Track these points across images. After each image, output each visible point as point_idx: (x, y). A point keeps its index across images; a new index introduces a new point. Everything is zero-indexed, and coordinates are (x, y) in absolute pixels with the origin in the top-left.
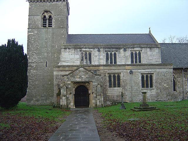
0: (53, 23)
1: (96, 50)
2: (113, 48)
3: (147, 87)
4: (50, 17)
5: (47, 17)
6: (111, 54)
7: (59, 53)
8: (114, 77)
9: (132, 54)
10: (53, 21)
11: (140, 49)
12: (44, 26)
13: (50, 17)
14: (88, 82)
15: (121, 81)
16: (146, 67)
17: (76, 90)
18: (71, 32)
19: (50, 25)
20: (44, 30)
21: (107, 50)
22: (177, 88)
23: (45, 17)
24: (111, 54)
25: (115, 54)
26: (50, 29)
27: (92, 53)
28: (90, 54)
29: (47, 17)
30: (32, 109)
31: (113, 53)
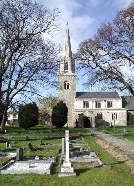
0: (69, 87)
1: (91, 101)
2: (99, 100)
3: (98, 107)
4: (68, 84)
5: (67, 84)
6: (98, 103)
7: (73, 102)
8: (100, 114)
9: (108, 103)
10: (70, 86)
11: (112, 101)
12: (65, 88)
13: (68, 84)
14: (90, 117)
15: (103, 116)
16: (114, 110)
17: (84, 121)
18: (126, 125)
19: (68, 88)
20: (65, 90)
21: (96, 101)
22: (130, 119)
23: (65, 83)
24: (98, 103)
25: (100, 103)
26: (68, 90)
27: (89, 103)
28: (88, 103)
29: (67, 84)
30: (6, 127)
31: (99, 102)
